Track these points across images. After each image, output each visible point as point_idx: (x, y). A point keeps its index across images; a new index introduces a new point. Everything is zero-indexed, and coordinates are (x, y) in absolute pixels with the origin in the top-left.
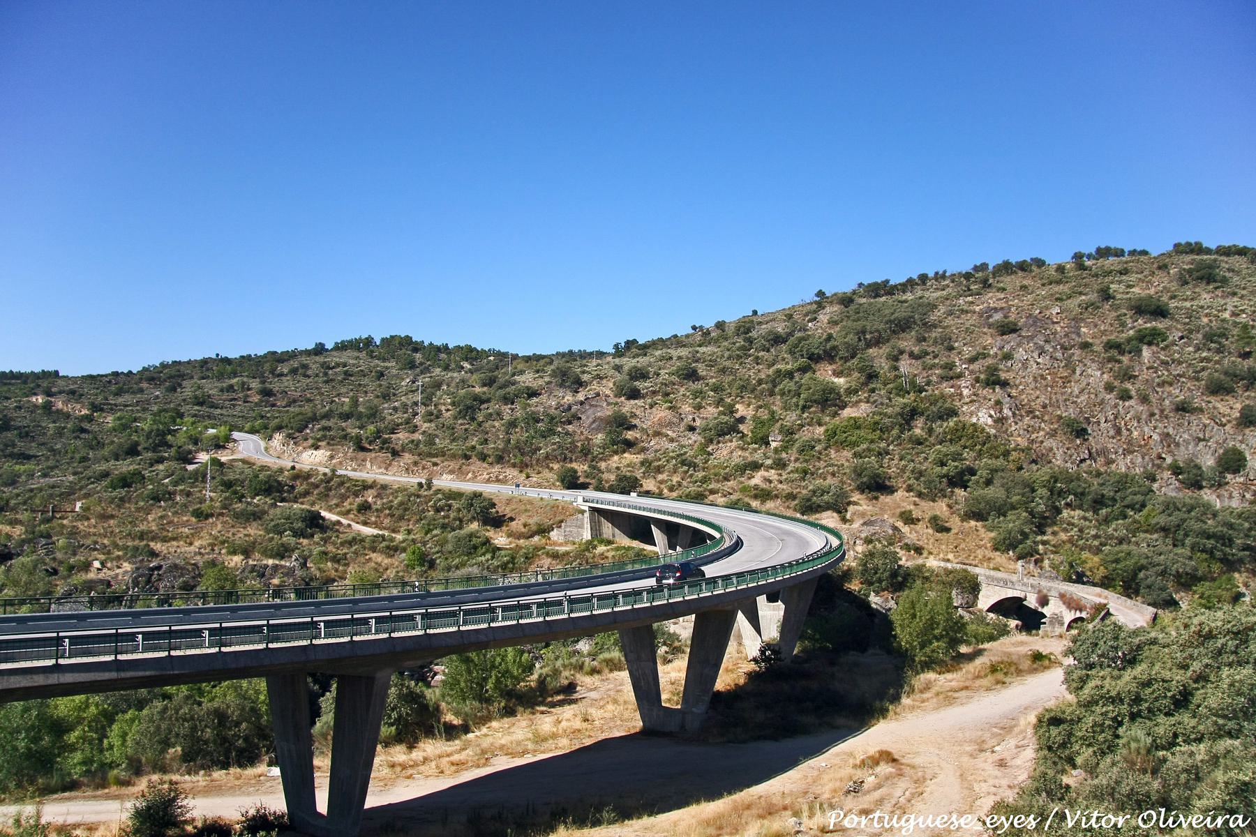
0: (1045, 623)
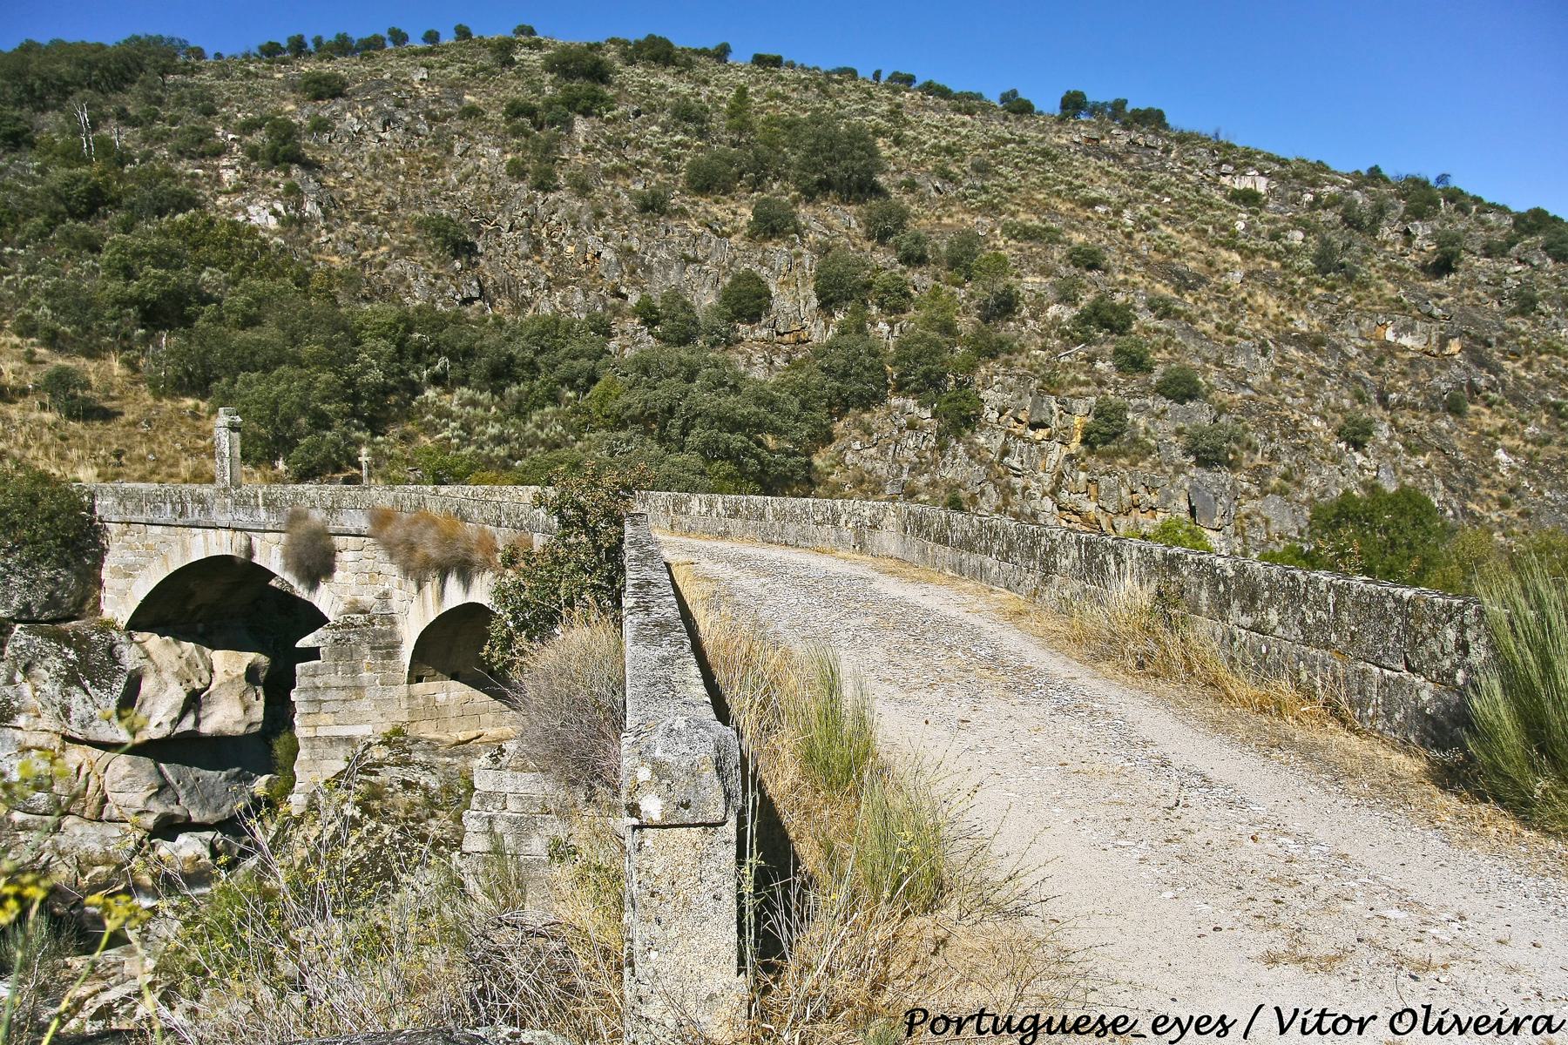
0: (312, 654)
